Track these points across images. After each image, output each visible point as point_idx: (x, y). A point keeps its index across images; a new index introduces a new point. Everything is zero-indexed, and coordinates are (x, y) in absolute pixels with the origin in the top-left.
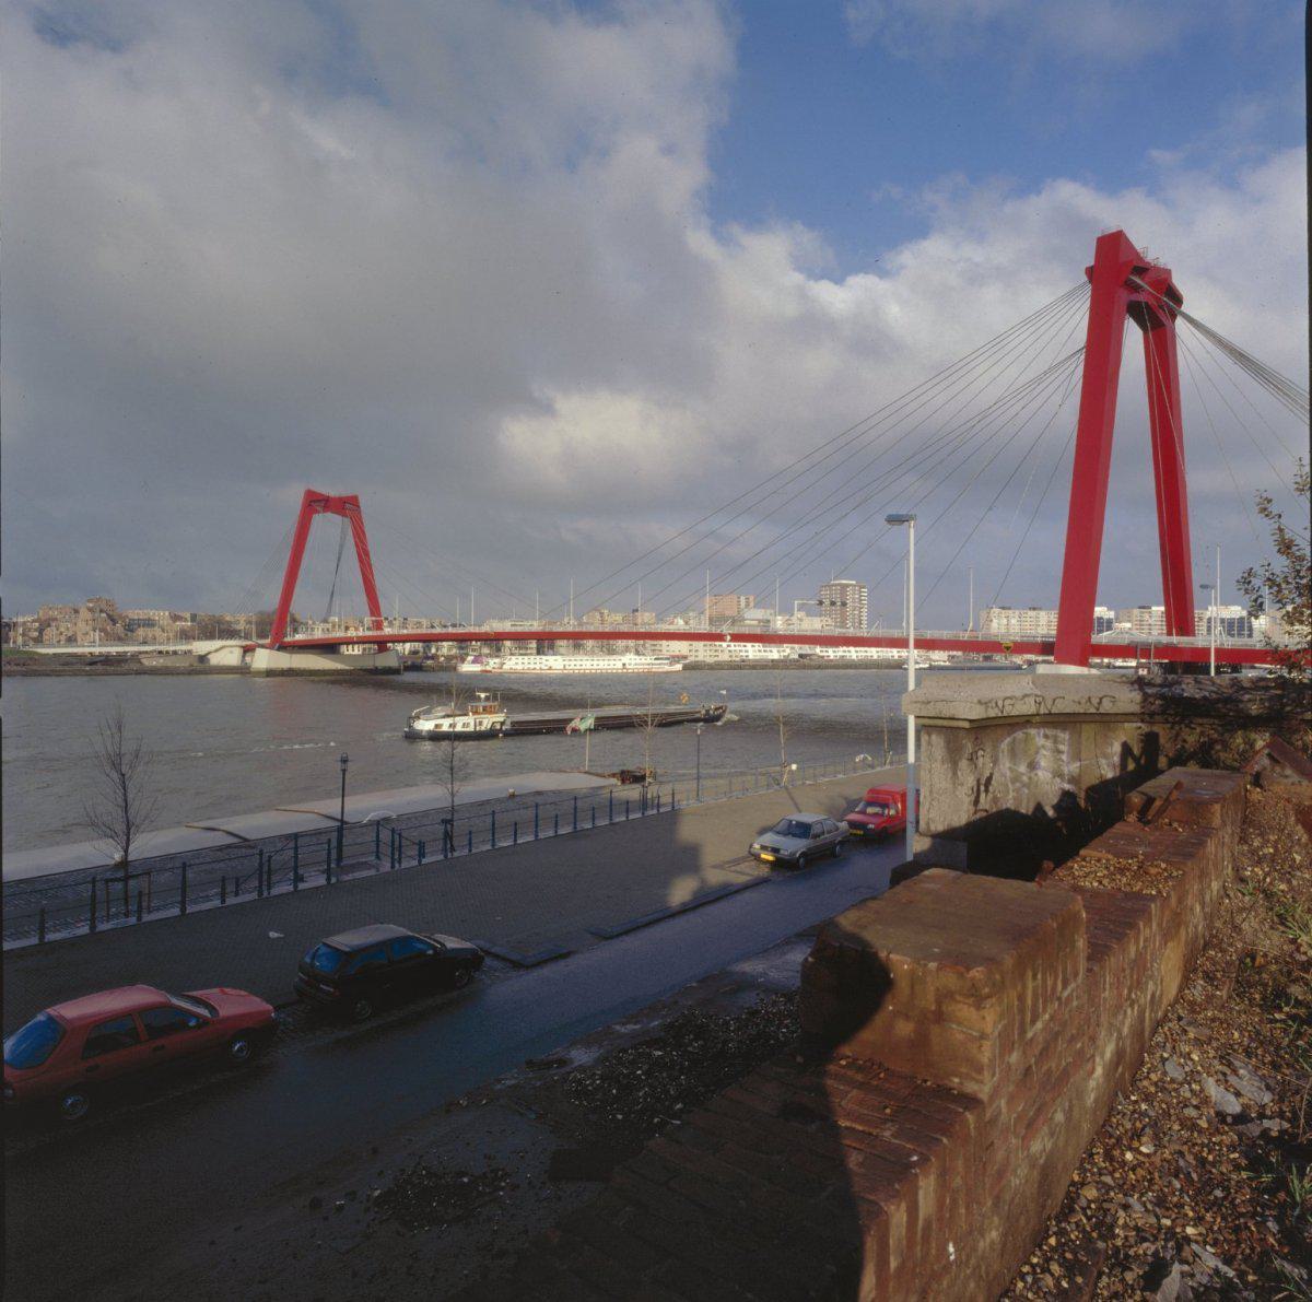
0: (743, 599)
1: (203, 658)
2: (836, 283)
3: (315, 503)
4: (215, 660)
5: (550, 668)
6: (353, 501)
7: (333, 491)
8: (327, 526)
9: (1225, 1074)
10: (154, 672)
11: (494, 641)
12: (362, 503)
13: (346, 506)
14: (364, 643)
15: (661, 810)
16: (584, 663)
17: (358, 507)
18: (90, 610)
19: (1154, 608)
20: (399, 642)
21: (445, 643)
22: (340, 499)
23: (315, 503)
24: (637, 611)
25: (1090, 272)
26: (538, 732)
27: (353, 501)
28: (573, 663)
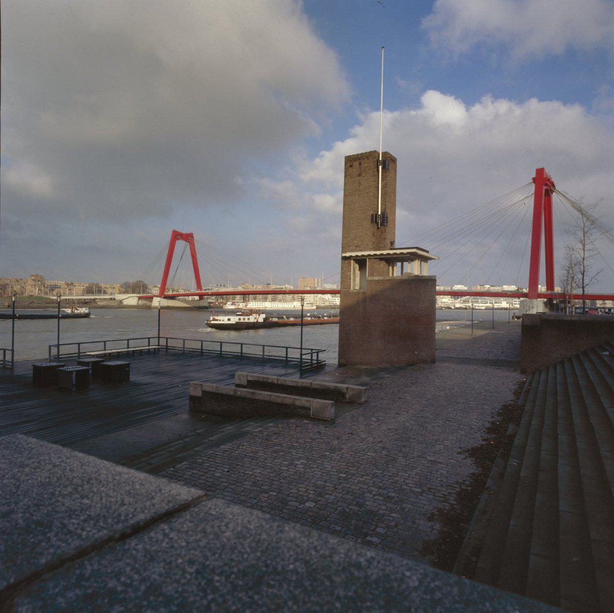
0: (316, 280)
1: (121, 302)
2: (350, 156)
3: (176, 236)
4: (125, 303)
5: (266, 307)
6: (191, 235)
7: (185, 231)
8: (180, 244)
9: (301, 503)
10: (102, 307)
11: (245, 295)
12: (196, 237)
13: (188, 238)
14: (264, 294)
15: (474, 322)
16: (278, 305)
17: (193, 238)
18: (34, 280)
19: (485, 286)
20: (225, 295)
21: (237, 296)
22: (186, 234)
23: (176, 236)
24: (269, 284)
25: (387, 152)
26: (328, 323)
27: (191, 235)
28: (274, 305)
